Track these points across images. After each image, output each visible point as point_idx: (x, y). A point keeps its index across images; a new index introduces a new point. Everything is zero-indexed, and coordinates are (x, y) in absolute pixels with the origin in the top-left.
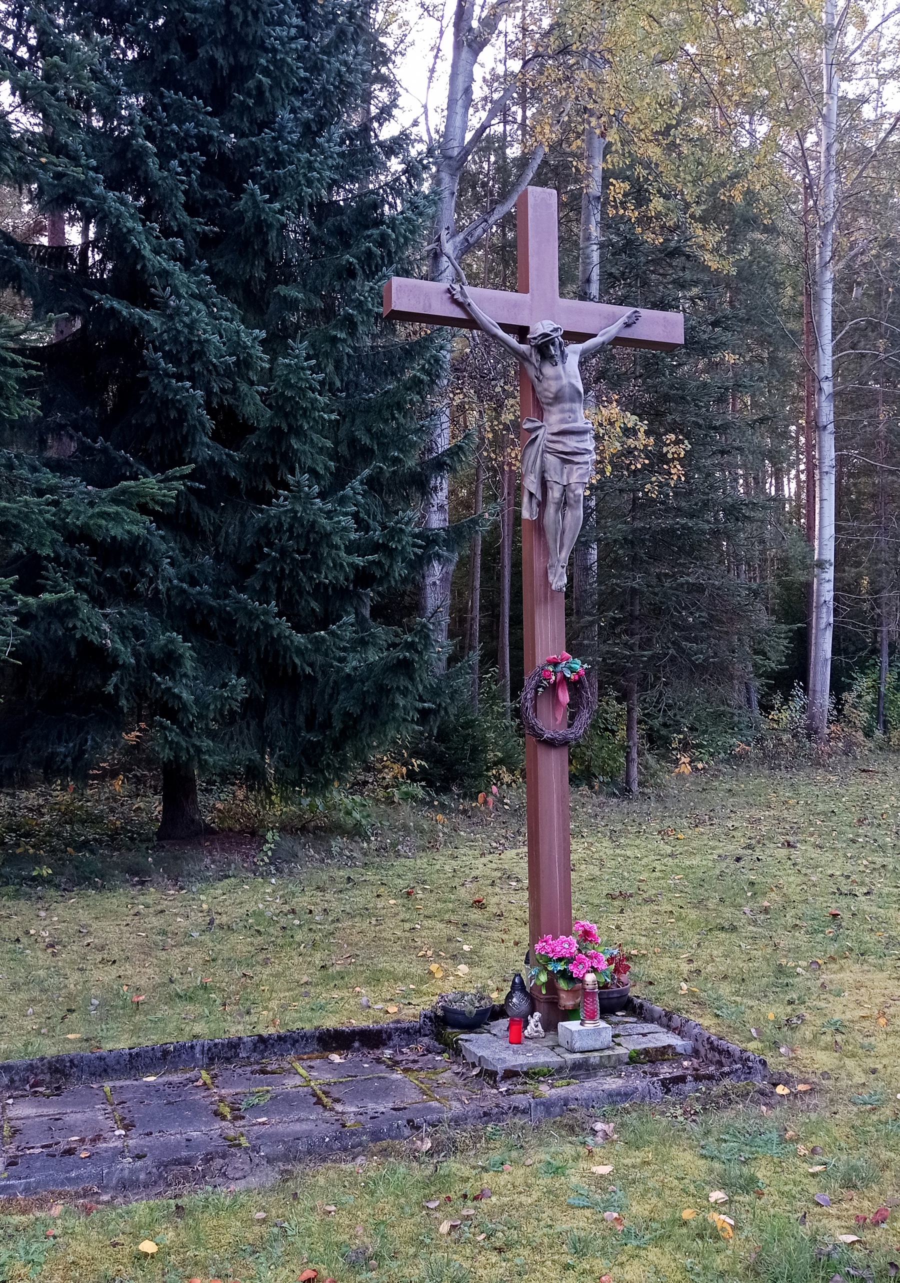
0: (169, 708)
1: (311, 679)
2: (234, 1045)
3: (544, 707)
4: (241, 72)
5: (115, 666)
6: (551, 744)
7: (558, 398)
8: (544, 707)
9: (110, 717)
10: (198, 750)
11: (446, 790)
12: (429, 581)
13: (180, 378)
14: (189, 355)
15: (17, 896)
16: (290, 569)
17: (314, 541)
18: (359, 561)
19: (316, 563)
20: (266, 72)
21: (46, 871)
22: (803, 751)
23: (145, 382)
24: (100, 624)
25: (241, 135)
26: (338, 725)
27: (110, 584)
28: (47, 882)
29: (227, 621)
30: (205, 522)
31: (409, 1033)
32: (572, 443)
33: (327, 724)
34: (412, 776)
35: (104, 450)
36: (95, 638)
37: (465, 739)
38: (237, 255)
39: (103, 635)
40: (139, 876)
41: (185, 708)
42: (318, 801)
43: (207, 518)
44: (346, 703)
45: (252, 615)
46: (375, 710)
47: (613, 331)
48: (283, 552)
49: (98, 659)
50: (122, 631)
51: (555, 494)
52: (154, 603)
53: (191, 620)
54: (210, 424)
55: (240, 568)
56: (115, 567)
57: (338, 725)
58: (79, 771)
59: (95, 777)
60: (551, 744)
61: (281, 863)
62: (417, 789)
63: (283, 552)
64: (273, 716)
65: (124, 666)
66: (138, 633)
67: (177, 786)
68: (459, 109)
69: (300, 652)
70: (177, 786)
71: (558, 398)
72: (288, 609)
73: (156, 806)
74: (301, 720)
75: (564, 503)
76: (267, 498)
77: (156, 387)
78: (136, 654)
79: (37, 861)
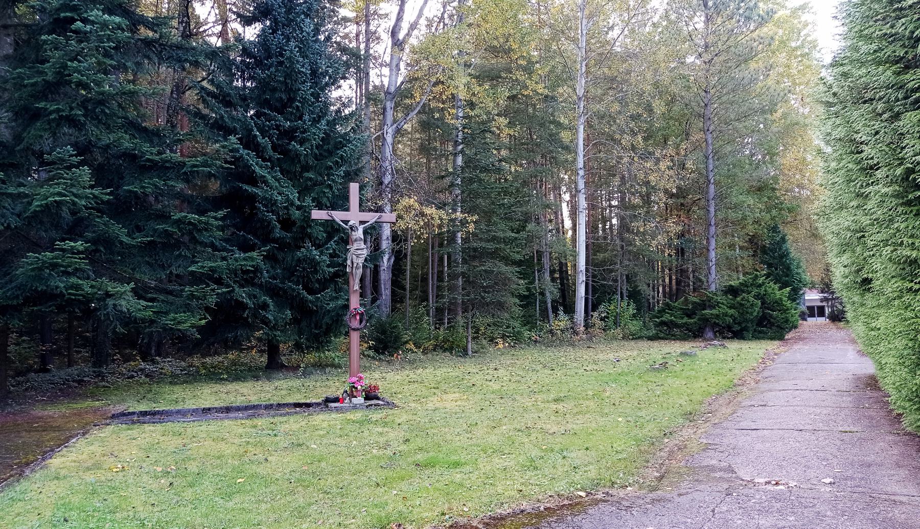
0: (265, 322)
1: (317, 311)
2: (272, 405)
3: (353, 320)
4: (292, 100)
5: (247, 308)
6: (354, 329)
7: (356, 240)
8: (353, 320)
9: (253, 328)
10: (275, 335)
11: (383, 353)
12: (382, 268)
13: (268, 212)
14: (271, 204)
15: (216, 383)
16: (308, 275)
17: (315, 264)
18: (331, 270)
19: (316, 272)
20: (300, 102)
21: (225, 376)
22: (569, 338)
23: (256, 214)
24: (242, 294)
25: (291, 121)
26: (324, 327)
27: (246, 280)
28: (226, 380)
29: (285, 292)
30: (280, 257)
31: (318, 404)
32: (359, 252)
33: (321, 327)
34: (370, 348)
35: (243, 235)
36: (240, 299)
37: (392, 332)
38: (288, 164)
39: (243, 298)
40: (257, 378)
41: (270, 321)
42: (322, 355)
43: (280, 256)
44: (327, 320)
45: (294, 290)
46: (337, 321)
47: (374, 220)
48: (304, 269)
49: (242, 306)
50: (250, 296)
51: (355, 265)
52: (260, 286)
53: (273, 292)
54: (279, 226)
55: (290, 273)
56: (248, 278)
57: (324, 327)
58: (236, 345)
59: (244, 349)
60: (354, 329)
61: (305, 374)
62: (371, 353)
63: (304, 269)
64: (304, 324)
65: (250, 308)
66: (255, 297)
67: (273, 351)
68: (394, 73)
69: (311, 301)
70: (273, 351)
71: (356, 240)
72: (305, 288)
73: (264, 359)
74: (313, 325)
75: (357, 268)
76: (299, 248)
77: (260, 215)
78: (254, 303)
79: (222, 373)
